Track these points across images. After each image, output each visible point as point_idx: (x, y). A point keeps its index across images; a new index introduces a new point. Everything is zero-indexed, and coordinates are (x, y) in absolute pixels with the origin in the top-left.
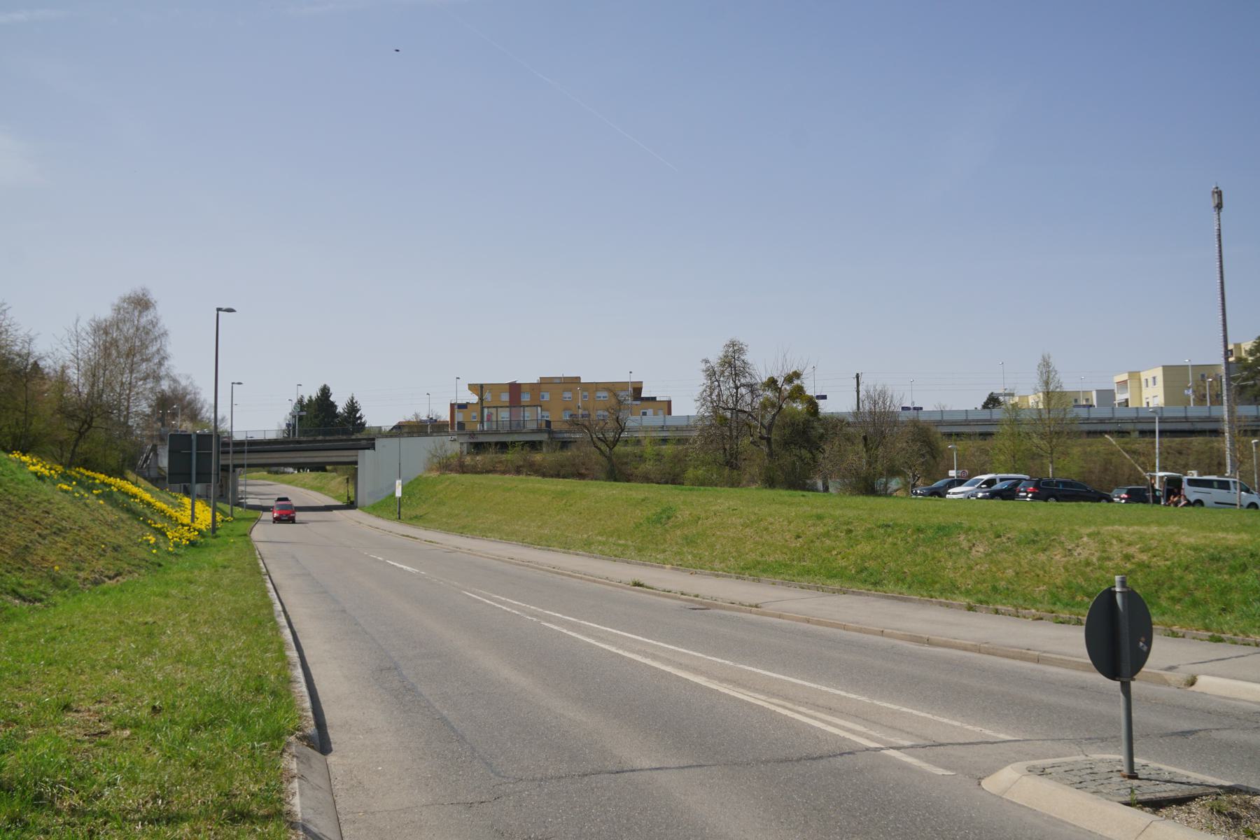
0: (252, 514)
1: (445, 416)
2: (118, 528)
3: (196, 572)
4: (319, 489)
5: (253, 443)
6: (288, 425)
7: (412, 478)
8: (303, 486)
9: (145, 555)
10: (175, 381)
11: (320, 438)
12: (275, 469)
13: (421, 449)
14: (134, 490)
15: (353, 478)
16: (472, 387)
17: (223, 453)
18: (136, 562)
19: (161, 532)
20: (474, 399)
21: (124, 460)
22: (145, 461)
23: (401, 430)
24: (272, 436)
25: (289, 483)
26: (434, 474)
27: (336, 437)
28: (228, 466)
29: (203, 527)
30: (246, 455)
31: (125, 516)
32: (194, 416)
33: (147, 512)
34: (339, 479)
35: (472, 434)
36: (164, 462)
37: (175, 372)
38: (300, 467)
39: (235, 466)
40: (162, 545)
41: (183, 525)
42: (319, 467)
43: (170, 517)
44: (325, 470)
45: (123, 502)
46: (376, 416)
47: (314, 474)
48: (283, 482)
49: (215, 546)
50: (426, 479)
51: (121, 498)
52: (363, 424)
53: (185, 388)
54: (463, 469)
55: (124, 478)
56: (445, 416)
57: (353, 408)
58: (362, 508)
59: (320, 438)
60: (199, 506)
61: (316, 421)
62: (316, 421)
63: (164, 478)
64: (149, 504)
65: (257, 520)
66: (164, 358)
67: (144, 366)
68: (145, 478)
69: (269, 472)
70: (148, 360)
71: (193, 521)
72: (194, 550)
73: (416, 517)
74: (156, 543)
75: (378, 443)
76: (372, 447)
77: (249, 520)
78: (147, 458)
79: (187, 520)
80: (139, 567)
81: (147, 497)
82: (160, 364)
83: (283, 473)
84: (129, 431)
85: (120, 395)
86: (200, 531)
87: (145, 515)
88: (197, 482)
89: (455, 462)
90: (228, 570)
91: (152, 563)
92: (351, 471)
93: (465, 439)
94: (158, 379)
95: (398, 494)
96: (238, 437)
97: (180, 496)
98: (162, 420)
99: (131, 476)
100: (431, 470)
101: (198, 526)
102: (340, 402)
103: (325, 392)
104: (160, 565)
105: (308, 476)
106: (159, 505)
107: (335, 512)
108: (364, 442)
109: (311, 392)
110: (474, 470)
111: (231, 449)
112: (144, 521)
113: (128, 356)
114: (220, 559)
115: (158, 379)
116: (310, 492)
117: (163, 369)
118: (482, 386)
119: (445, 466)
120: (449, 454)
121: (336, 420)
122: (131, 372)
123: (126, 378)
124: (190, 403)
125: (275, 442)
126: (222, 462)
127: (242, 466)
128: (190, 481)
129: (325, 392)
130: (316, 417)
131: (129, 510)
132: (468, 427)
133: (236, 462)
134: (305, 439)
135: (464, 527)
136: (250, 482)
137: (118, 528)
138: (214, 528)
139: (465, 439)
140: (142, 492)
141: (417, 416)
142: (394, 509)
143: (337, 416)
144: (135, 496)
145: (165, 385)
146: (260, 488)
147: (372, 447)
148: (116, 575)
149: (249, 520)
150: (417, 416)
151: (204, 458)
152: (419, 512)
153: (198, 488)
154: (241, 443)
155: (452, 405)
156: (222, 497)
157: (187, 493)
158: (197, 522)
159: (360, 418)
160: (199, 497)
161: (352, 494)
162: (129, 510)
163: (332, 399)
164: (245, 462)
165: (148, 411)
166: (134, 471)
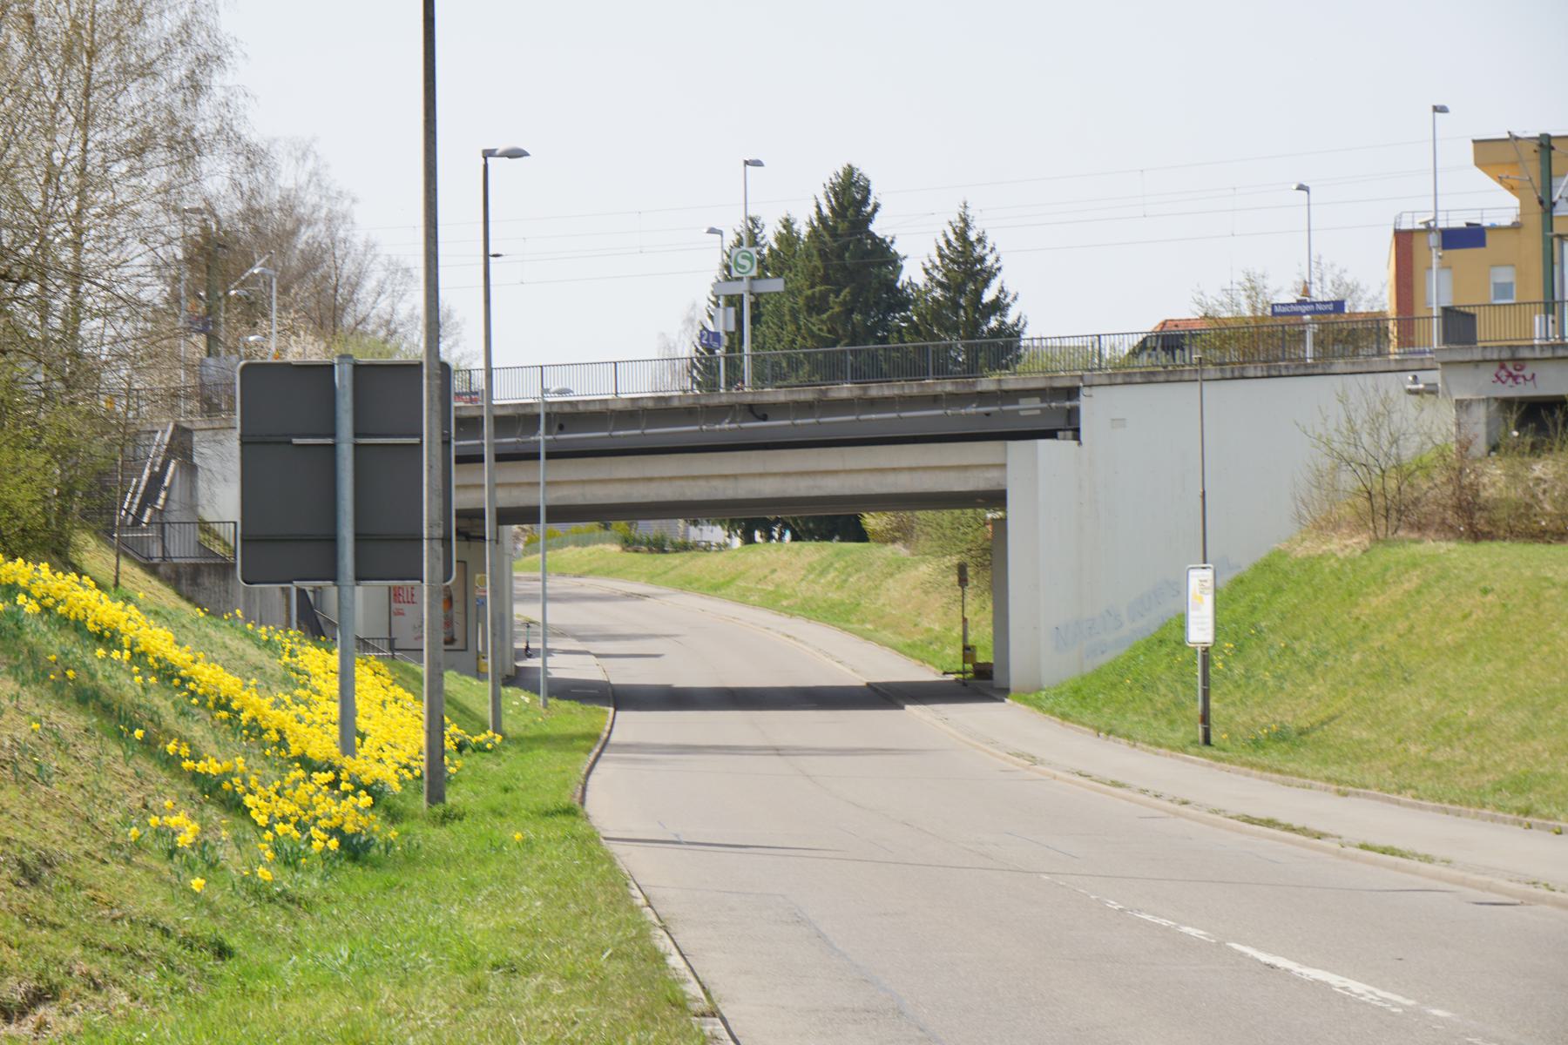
0: (574, 718)
1: (1374, 290)
2: (42, 776)
3: (387, 992)
4: (835, 615)
5: (567, 417)
6: (709, 340)
7: (1244, 562)
8: (772, 601)
9: (153, 902)
10: (254, 157)
11: (845, 390)
12: (650, 528)
13: (1289, 430)
14: (104, 610)
15: (986, 564)
16: (1492, 154)
17: (461, 460)
18: (119, 935)
19: (221, 796)
20: (1494, 204)
21: (67, 492)
22: (149, 498)
23: (1170, 351)
24: (639, 386)
25: (714, 589)
26: (1346, 545)
27: (912, 388)
28: (479, 514)
29: (387, 774)
30: (542, 470)
31: (70, 721)
32: (328, 313)
33: (163, 704)
34: (925, 570)
35: (1512, 362)
36: (222, 499)
37: (257, 128)
38: (753, 519)
39: (507, 516)
40: (227, 854)
41: (308, 765)
42: (835, 521)
43: (256, 729)
44: (857, 534)
45: (65, 661)
46: (1059, 302)
47: (812, 551)
48: (687, 584)
49: (449, 861)
50: (1310, 565)
51: (55, 644)
52: (1010, 336)
53: (288, 206)
54: (1473, 520)
55: (64, 560)
56: (1374, 290)
57: (966, 265)
58: (1032, 696)
59: (845, 390)
60: (370, 681)
61: (818, 324)
62: (818, 324)
63: (224, 569)
64: (168, 674)
65: (598, 743)
66: (204, 61)
67: (132, 97)
68: (151, 569)
69: (630, 544)
70: (146, 70)
71: (348, 748)
72: (359, 879)
73: (1280, 736)
74: (200, 845)
75: (1094, 408)
76: (1070, 426)
77: (565, 742)
78: (156, 480)
79: (323, 744)
80: (133, 956)
81: (159, 640)
82: (194, 87)
83: (685, 547)
84: (76, 371)
85: (48, 218)
86: (376, 791)
87: (155, 718)
88: (359, 577)
89: (1435, 489)
90: (528, 987)
91: (189, 942)
92: (978, 534)
93: (1483, 385)
94: (186, 148)
95: (1200, 630)
96: (511, 392)
97: (290, 638)
98: (206, 325)
99: (95, 554)
100: (1326, 525)
101: (364, 765)
102: (915, 248)
103: (851, 200)
104: (222, 952)
105: (786, 559)
106: (212, 676)
107: (913, 711)
108: (1029, 407)
109: (798, 203)
110: (1525, 527)
111: (487, 442)
112: (149, 744)
113: (69, 56)
114: (480, 925)
115: (186, 148)
116: (799, 626)
117: (206, 106)
118: (1546, 144)
119: (1394, 511)
120: (1408, 451)
121: (897, 319)
122: (85, 123)
123: (65, 147)
124: (312, 261)
125: (659, 411)
126: (460, 500)
127: (526, 515)
128: (333, 576)
129: (851, 200)
130: (816, 306)
131: (87, 697)
132: (1491, 331)
133: (507, 499)
134: (782, 396)
135: (1519, 785)
136: (556, 584)
137: (42, 776)
138: (436, 782)
139: (1483, 385)
140: (139, 617)
141: (1253, 290)
142: (1180, 695)
143: (898, 299)
144: (107, 638)
145: (216, 179)
146: (583, 602)
147: (1070, 426)
148: (38, 997)
149: (565, 742)
150: (1253, 290)
151: (386, 469)
152: (1291, 713)
153: (361, 602)
154: (519, 420)
155: (1404, 241)
156: (455, 643)
157: (314, 626)
158: (367, 749)
159: (998, 306)
160: (364, 645)
161: (981, 636)
162: (87, 697)
163: (876, 227)
164: (541, 498)
165: (154, 292)
166: (106, 534)
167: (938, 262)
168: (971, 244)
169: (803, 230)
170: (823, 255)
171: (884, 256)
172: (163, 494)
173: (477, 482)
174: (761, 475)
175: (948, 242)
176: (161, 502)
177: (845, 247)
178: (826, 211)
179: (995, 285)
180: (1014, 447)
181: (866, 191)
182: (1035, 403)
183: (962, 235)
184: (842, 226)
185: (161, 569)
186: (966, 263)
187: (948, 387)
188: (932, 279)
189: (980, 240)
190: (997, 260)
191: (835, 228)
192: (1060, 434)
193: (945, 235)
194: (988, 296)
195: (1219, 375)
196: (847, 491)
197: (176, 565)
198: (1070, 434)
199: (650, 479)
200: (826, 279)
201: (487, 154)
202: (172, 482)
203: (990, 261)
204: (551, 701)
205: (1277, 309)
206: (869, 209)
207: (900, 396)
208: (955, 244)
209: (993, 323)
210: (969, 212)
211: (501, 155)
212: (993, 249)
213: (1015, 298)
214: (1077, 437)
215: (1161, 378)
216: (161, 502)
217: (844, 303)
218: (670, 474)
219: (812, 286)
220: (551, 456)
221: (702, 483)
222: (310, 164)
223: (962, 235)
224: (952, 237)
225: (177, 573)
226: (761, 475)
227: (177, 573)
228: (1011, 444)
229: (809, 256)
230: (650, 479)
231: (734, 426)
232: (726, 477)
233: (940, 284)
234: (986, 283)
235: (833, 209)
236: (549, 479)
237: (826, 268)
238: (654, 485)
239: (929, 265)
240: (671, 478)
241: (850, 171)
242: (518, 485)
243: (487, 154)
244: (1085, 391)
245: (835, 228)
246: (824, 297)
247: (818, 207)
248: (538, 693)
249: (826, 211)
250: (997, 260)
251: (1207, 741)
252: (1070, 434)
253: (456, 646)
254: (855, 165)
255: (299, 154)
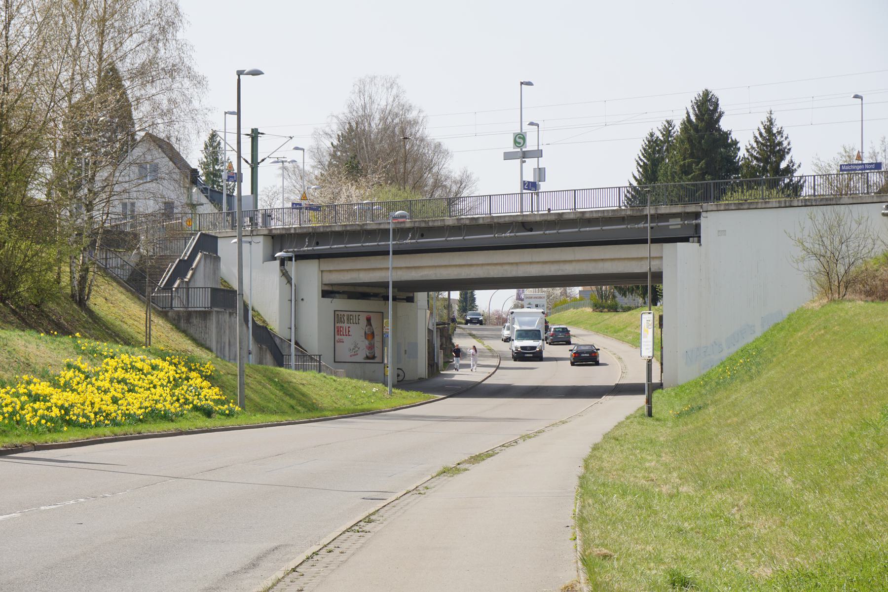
30: (391, 261)
103: (707, 109)
109: (678, 111)
129: (707, 109)
130: (686, 171)
159: (789, 171)
167: (755, 145)
168: (774, 134)
169: (677, 128)
170: (690, 140)
171: (724, 143)
172: (190, 272)
173: (386, 266)
174: (531, 263)
175: (761, 134)
176: (189, 276)
177: (702, 137)
178: (693, 118)
179: (788, 158)
180: (667, 246)
181: (716, 105)
182: (678, 221)
183: (769, 130)
184: (701, 125)
185: (170, 314)
186: (770, 146)
187: (236, 189)
188: (752, 155)
189: (779, 133)
190: (789, 144)
191: (697, 126)
192: (691, 239)
193: (759, 129)
194: (783, 165)
195: (777, 205)
196: (560, 273)
197: (178, 312)
198: (696, 239)
199: (471, 265)
200: (692, 155)
201: (240, 73)
202: (197, 266)
203: (785, 143)
204: (393, 390)
205: (843, 168)
206: (717, 115)
207: (603, 218)
208: (765, 134)
209: (787, 181)
210: (773, 116)
211: (248, 74)
212: (786, 138)
213: (799, 166)
214: (699, 241)
215: (746, 207)
216: (189, 276)
217: (701, 169)
218: (481, 262)
219: (684, 159)
220: (395, 253)
221: (499, 267)
222: (394, 91)
223: (769, 130)
224: (763, 131)
225: (179, 316)
226: (531, 263)
227: (179, 316)
228: (679, 244)
229: (682, 142)
230: (471, 265)
231: (512, 234)
232: (512, 264)
233: (756, 158)
234: (782, 158)
235: (696, 115)
236: (395, 266)
237: (692, 149)
238: (473, 269)
239: (749, 147)
240: (483, 265)
241: (706, 93)
242: (401, 268)
243: (240, 73)
244: (703, 214)
245: (697, 126)
246: (690, 165)
247: (688, 113)
248: (386, 385)
249: (693, 118)
250: (789, 144)
251: (650, 414)
252: (696, 239)
253: (376, 360)
254: (709, 90)
255: (389, 85)
